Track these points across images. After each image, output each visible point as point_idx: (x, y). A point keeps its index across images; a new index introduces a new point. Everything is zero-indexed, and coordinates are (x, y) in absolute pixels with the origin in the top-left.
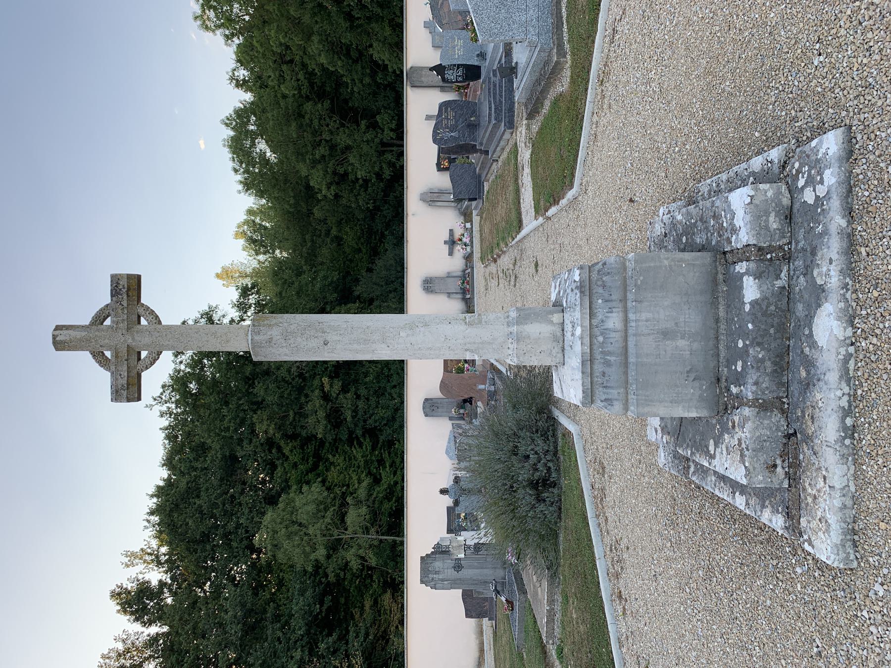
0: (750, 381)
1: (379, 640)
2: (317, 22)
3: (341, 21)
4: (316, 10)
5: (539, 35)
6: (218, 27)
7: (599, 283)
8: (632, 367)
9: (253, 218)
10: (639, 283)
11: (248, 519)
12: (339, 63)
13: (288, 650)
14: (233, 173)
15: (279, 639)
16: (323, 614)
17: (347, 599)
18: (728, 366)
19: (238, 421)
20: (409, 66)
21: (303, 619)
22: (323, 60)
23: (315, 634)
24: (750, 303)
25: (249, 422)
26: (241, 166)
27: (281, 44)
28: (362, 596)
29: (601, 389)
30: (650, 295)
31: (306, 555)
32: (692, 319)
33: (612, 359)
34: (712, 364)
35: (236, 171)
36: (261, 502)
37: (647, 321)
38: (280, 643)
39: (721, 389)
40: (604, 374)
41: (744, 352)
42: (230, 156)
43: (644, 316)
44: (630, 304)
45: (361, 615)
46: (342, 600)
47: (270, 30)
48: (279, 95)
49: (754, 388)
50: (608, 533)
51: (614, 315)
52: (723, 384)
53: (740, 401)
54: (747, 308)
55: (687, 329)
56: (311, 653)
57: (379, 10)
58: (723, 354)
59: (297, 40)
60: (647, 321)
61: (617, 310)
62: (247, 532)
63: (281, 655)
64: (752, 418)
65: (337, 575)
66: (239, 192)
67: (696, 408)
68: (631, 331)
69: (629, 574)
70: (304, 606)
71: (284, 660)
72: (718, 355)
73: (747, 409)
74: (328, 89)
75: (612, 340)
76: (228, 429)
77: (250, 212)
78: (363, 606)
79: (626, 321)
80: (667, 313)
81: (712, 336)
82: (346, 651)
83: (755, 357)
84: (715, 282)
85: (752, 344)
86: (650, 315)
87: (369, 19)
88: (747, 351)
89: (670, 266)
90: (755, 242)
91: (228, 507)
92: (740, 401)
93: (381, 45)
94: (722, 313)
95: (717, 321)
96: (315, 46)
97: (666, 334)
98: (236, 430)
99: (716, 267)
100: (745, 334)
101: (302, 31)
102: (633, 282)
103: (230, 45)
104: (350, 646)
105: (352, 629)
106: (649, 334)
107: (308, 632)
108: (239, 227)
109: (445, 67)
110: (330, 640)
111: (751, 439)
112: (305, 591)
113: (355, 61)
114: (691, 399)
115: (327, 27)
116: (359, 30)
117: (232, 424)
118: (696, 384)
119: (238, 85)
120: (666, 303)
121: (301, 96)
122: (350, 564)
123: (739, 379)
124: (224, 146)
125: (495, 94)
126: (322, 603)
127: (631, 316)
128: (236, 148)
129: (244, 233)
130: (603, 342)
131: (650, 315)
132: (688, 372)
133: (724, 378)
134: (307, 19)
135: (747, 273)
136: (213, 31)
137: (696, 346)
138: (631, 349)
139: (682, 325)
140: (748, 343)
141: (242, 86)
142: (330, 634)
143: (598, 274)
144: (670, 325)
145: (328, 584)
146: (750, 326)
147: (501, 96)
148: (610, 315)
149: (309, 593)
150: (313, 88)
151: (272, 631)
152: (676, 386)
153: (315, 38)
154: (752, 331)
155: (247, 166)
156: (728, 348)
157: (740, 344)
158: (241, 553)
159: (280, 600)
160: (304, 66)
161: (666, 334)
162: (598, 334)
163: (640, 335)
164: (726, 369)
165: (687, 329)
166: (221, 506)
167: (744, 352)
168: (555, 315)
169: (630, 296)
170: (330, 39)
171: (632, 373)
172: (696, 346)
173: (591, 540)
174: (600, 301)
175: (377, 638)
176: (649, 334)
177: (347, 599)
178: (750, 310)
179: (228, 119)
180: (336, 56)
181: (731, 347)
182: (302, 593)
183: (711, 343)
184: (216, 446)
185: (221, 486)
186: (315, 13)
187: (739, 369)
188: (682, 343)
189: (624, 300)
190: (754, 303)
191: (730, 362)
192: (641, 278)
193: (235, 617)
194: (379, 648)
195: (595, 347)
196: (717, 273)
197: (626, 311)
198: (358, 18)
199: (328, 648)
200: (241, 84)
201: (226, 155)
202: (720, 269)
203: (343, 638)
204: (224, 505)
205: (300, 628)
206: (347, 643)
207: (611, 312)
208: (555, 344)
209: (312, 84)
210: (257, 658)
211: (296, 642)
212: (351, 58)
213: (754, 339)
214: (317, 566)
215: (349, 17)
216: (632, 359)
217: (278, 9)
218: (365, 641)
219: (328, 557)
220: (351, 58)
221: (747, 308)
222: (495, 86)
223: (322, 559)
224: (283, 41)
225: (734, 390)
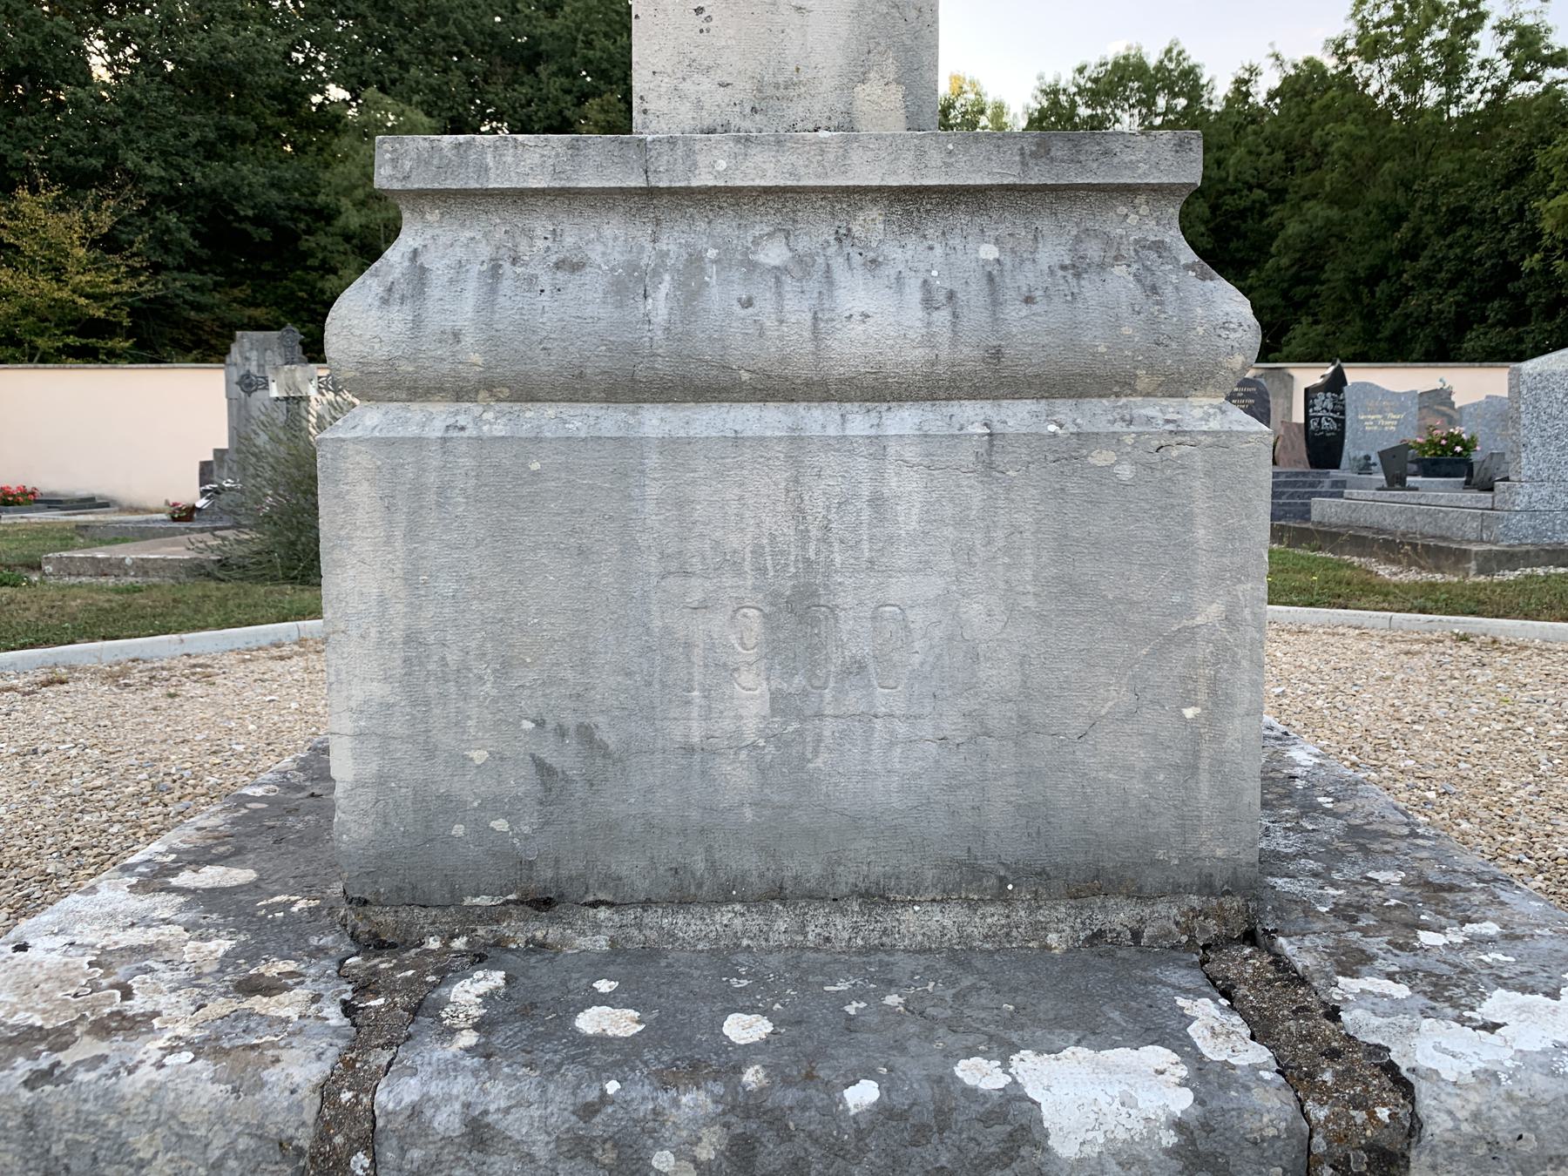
0: (497, 1095)
1: (193, 334)
2: (1368, 214)
3: (1368, 260)
4: (1391, 210)
5: (1531, 511)
6: (1362, 25)
7: (1093, 250)
8: (609, 420)
9: (989, 112)
10: (1101, 458)
11: (418, 83)
12: (1285, 262)
13: (162, 153)
14: (1077, 65)
15: (185, 135)
16: (236, 225)
17: (270, 276)
18: (617, 957)
19: (605, 65)
20: (1293, 372)
21: (225, 183)
22: (1293, 228)
23: (197, 208)
24: (1014, 1096)
25: (603, 87)
26: (1089, 79)
27: (1326, 145)
28: (276, 304)
29: (485, 251)
30: (1025, 519)
31: (348, 191)
32: (889, 755)
33: (660, 304)
34: (630, 867)
35: (1081, 71)
36: (451, 108)
37: (877, 501)
38: (176, 137)
39: (492, 916)
40: (572, 266)
41: (683, 1052)
42: (1110, 59)
43: (907, 488)
44: (972, 415)
45: (235, 300)
46: (266, 267)
47: (1355, 122)
48: (1221, 154)
49: (447, 1120)
50: (244, 661)
51: (914, 314)
52: (518, 931)
53: (384, 1016)
54: (980, 1074)
55: (829, 728)
56: (153, 198)
57: (1386, 333)
58: (688, 925)
59: (1332, 177)
60: (877, 501)
61: (945, 337)
62: (393, 82)
63: (153, 140)
64: (246, 1109)
65: (310, 254)
66: (1041, 78)
67: (382, 780)
68: (818, 419)
69: (104, 694)
70: (249, 185)
71: (143, 144)
72: (682, 902)
73: (316, 1071)
74: (1233, 245)
75: (765, 304)
76: (589, 44)
77: (999, 109)
78: (257, 306)
79: (878, 390)
80: (916, 617)
81: (792, 867)
82: (166, 268)
83: (652, 1129)
84: (1090, 885)
85: (745, 1107)
86: (908, 518)
87: (1369, 316)
88: (693, 1072)
89: (1189, 636)
90: (1438, 1125)
91: (440, 46)
92: (384, 1016)
93: (1320, 338)
94: (919, 922)
95: (875, 897)
96: (1318, 211)
97: (799, 611)
98: (587, 62)
99: (1177, 890)
100: (805, 1056)
101: (1347, 191)
102: (1102, 426)
103: (1325, 48)
104: (175, 274)
105: (209, 279)
106: (799, 514)
107: (200, 193)
108: (973, 84)
109: (1340, 392)
110: (185, 235)
111: (108, 1099)
112: (282, 190)
113: (1285, 295)
114: (430, 753)
115: (1355, 234)
116: (1348, 296)
117: (598, 54)
118: (520, 781)
119: (1240, 82)
120: (974, 611)
121: (1220, 195)
122: (331, 277)
123: (529, 1023)
124: (1129, 48)
125: (1294, 484)
126: (258, 221)
127: (903, 420)
128: (1125, 67)
129: (961, 92)
130: (752, 266)
131: (908, 518)
132: (586, 734)
133: (553, 933)
134: (1375, 193)
135: (1206, 1076)
136: (1354, 15)
137: (737, 775)
138: (709, 420)
139: (854, 701)
140: (752, 1077)
141: (1237, 89)
142: (195, 234)
143: (1141, 245)
144: (852, 634)
145: (296, 238)
146: (862, 1095)
147: (1292, 496)
148: (914, 295)
149: (275, 196)
150: (1234, 218)
151: (201, 125)
152: (506, 667)
153: (1335, 213)
154: (832, 1110)
155: (1090, 89)
156: (723, 957)
157: (743, 1029)
158: (354, 70)
159: (265, 146)
160: (1279, 195)
161: (799, 611)
162: (803, 244)
163: (794, 461)
164: (602, 943)
165: (829, 728)
166: (442, 32)
167: (683, 1052)
168: (896, 95)
169: (1017, 416)
170: (1332, 241)
171: (580, 420)
172: (737, 775)
173: (239, 624)
174: (989, 252)
175: (196, 327)
176: (799, 514)
177: (270, 276)
178: (971, 1093)
179: (1180, 53)
180: (1298, 255)
181: (726, 977)
182: (276, 184)
183: (746, 862)
184: (555, 26)
185: (481, 32)
186: (1386, 208)
187: (589, 1021)
188: (750, 697)
189: (996, 379)
190: (1016, 1123)
191: (637, 970)
192: (1126, 472)
193: (224, 49)
194: (176, 333)
195: (725, 226)
196: (1140, 895)
197: (933, 388)
198: (1373, 294)
199: (168, 230)
200: (1241, 89)
201: (1115, 50)
202: (1164, 915)
203: (192, 263)
204: (444, 38)
205: (204, 176)
206: (180, 269)
207: (928, 303)
208: (743, 90)
209: (1242, 214)
210: (144, 91)
211: (178, 168)
212: (1291, 287)
213: (776, 1120)
214: (326, 216)
215: (1376, 275)
216: (655, 421)
217: (1395, 140)
218: (185, 302)
219: (348, 237)
220: (1291, 287)
221: (980, 1074)
222: (1312, 485)
223: (340, 222)
224: (1333, 148)
225: (468, 993)
